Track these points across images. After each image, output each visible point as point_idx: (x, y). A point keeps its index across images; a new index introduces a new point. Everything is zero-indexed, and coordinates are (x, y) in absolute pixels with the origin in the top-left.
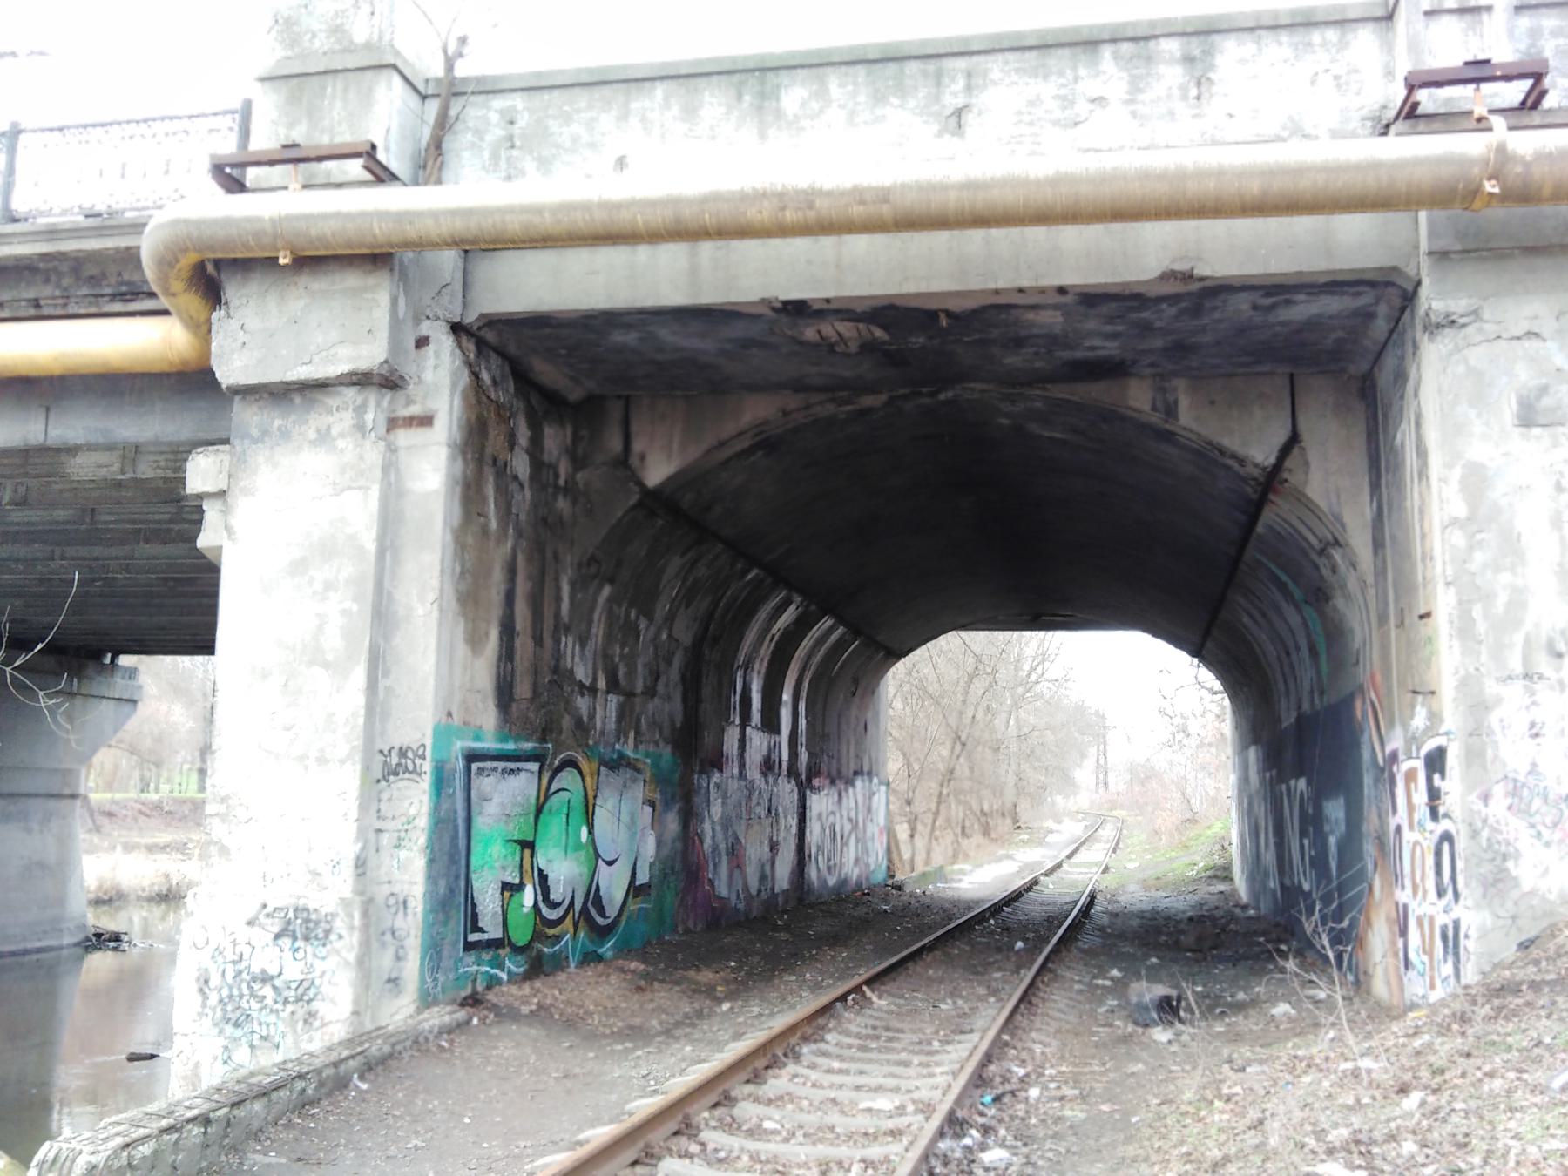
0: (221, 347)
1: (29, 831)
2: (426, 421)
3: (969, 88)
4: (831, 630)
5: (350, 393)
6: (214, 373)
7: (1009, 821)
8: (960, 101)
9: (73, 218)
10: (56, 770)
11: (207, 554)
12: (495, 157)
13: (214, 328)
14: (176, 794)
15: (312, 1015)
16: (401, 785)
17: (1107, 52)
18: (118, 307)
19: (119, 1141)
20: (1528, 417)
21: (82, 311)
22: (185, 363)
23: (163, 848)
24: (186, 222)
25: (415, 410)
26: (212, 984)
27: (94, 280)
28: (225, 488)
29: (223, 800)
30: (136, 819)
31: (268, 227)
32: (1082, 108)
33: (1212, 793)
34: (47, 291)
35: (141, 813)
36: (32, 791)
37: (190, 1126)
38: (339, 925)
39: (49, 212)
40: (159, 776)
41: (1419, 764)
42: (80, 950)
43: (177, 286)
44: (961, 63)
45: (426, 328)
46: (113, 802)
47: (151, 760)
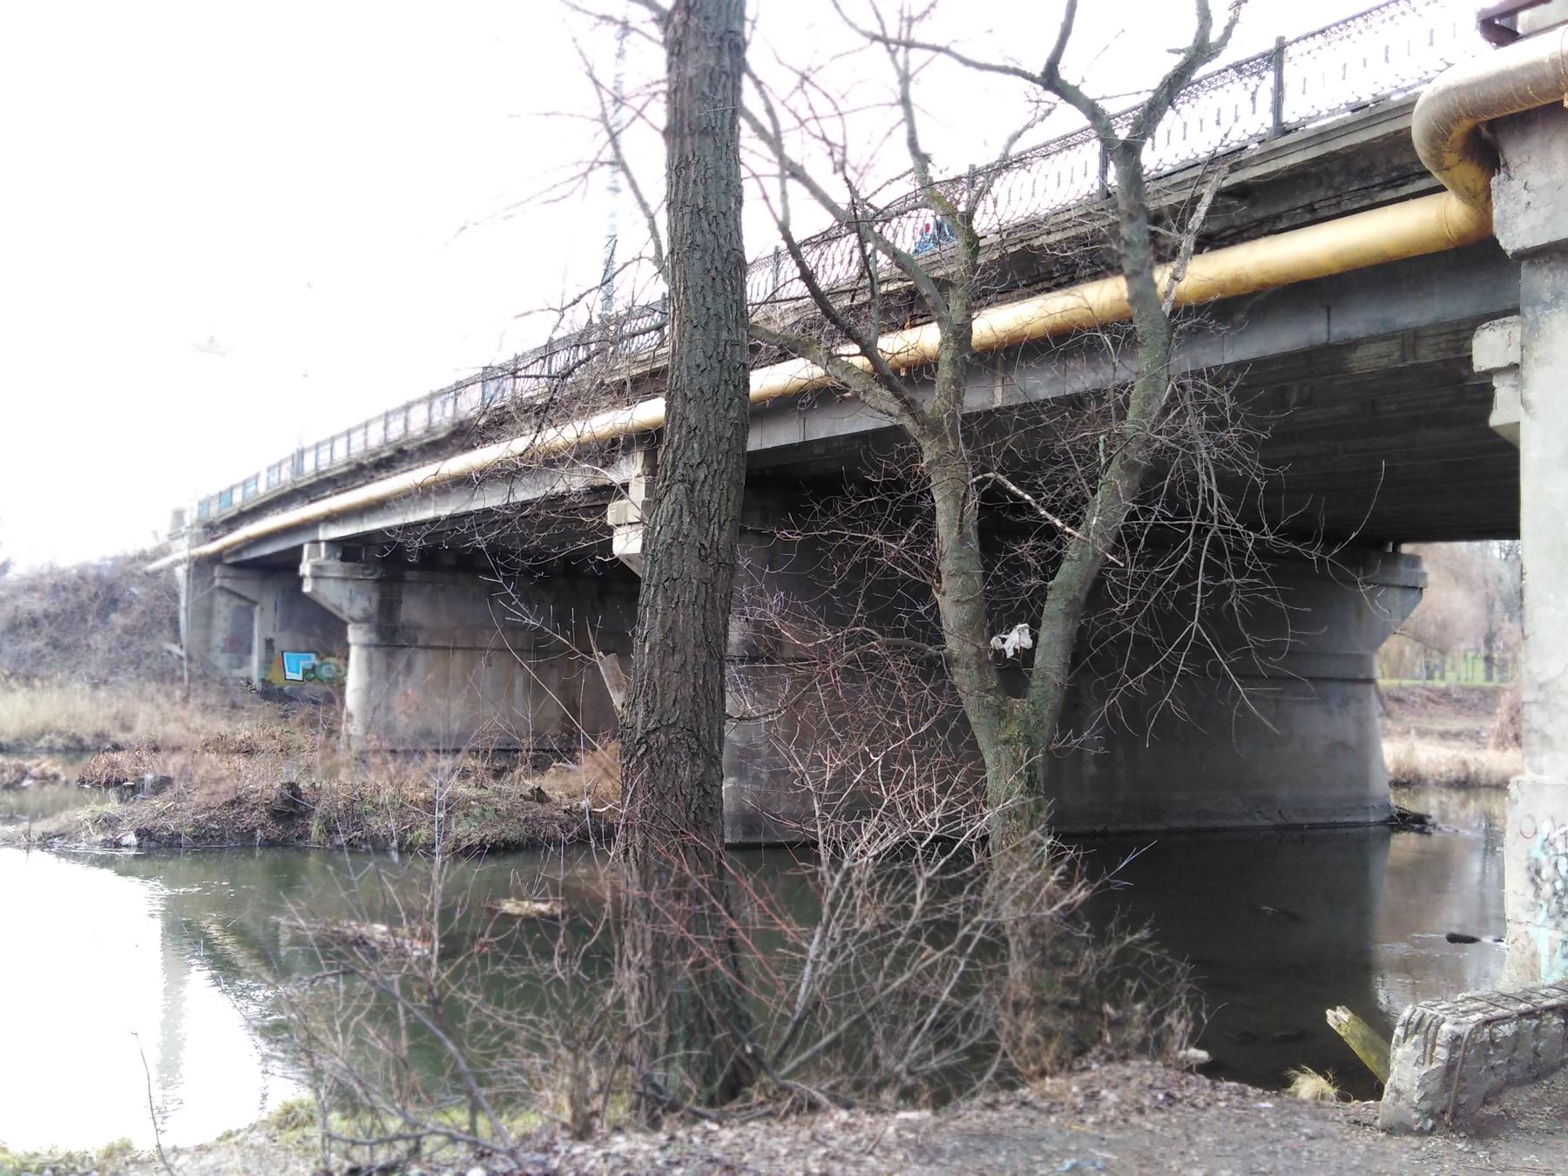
0: (1503, 212)
1: (1330, 712)
6: (1497, 241)
9: (1341, 116)
10: (1350, 656)
11: (1499, 431)
13: (1494, 193)
14: (1462, 682)
18: (1389, 194)
19: (1478, 1016)
21: (1356, 206)
22: (1463, 237)
23: (1457, 735)
24: (1457, 89)
26: (1544, 875)
27: (1365, 174)
28: (1517, 361)
29: (1541, 687)
30: (1424, 706)
31: (1549, 70)
34: (1321, 194)
35: (1429, 699)
36: (1330, 675)
37: (1549, 1015)
39: (1319, 116)
40: (1444, 662)
42: (1386, 829)
43: (1451, 158)
46: (1401, 688)
47: (1436, 646)
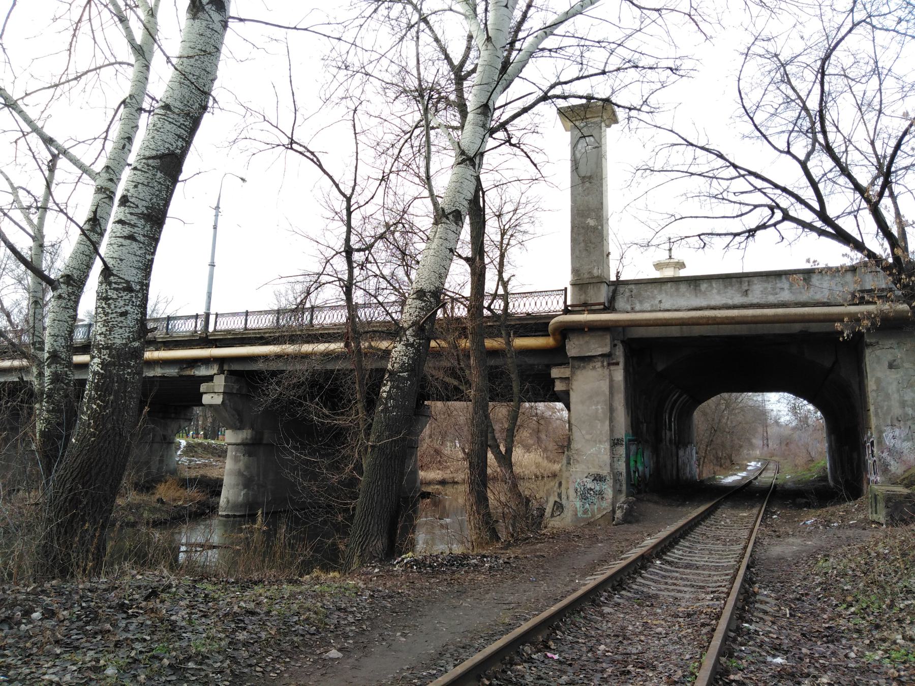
2: (617, 364)
3: (749, 285)
4: (679, 397)
5: (600, 358)
7: (729, 461)
8: (746, 288)
12: (628, 300)
15: (603, 498)
16: (618, 447)
17: (784, 277)
20: (891, 366)
25: (614, 361)
32: (778, 290)
33: (820, 450)
38: (608, 478)
41: (869, 444)
44: (746, 279)
45: (616, 342)
